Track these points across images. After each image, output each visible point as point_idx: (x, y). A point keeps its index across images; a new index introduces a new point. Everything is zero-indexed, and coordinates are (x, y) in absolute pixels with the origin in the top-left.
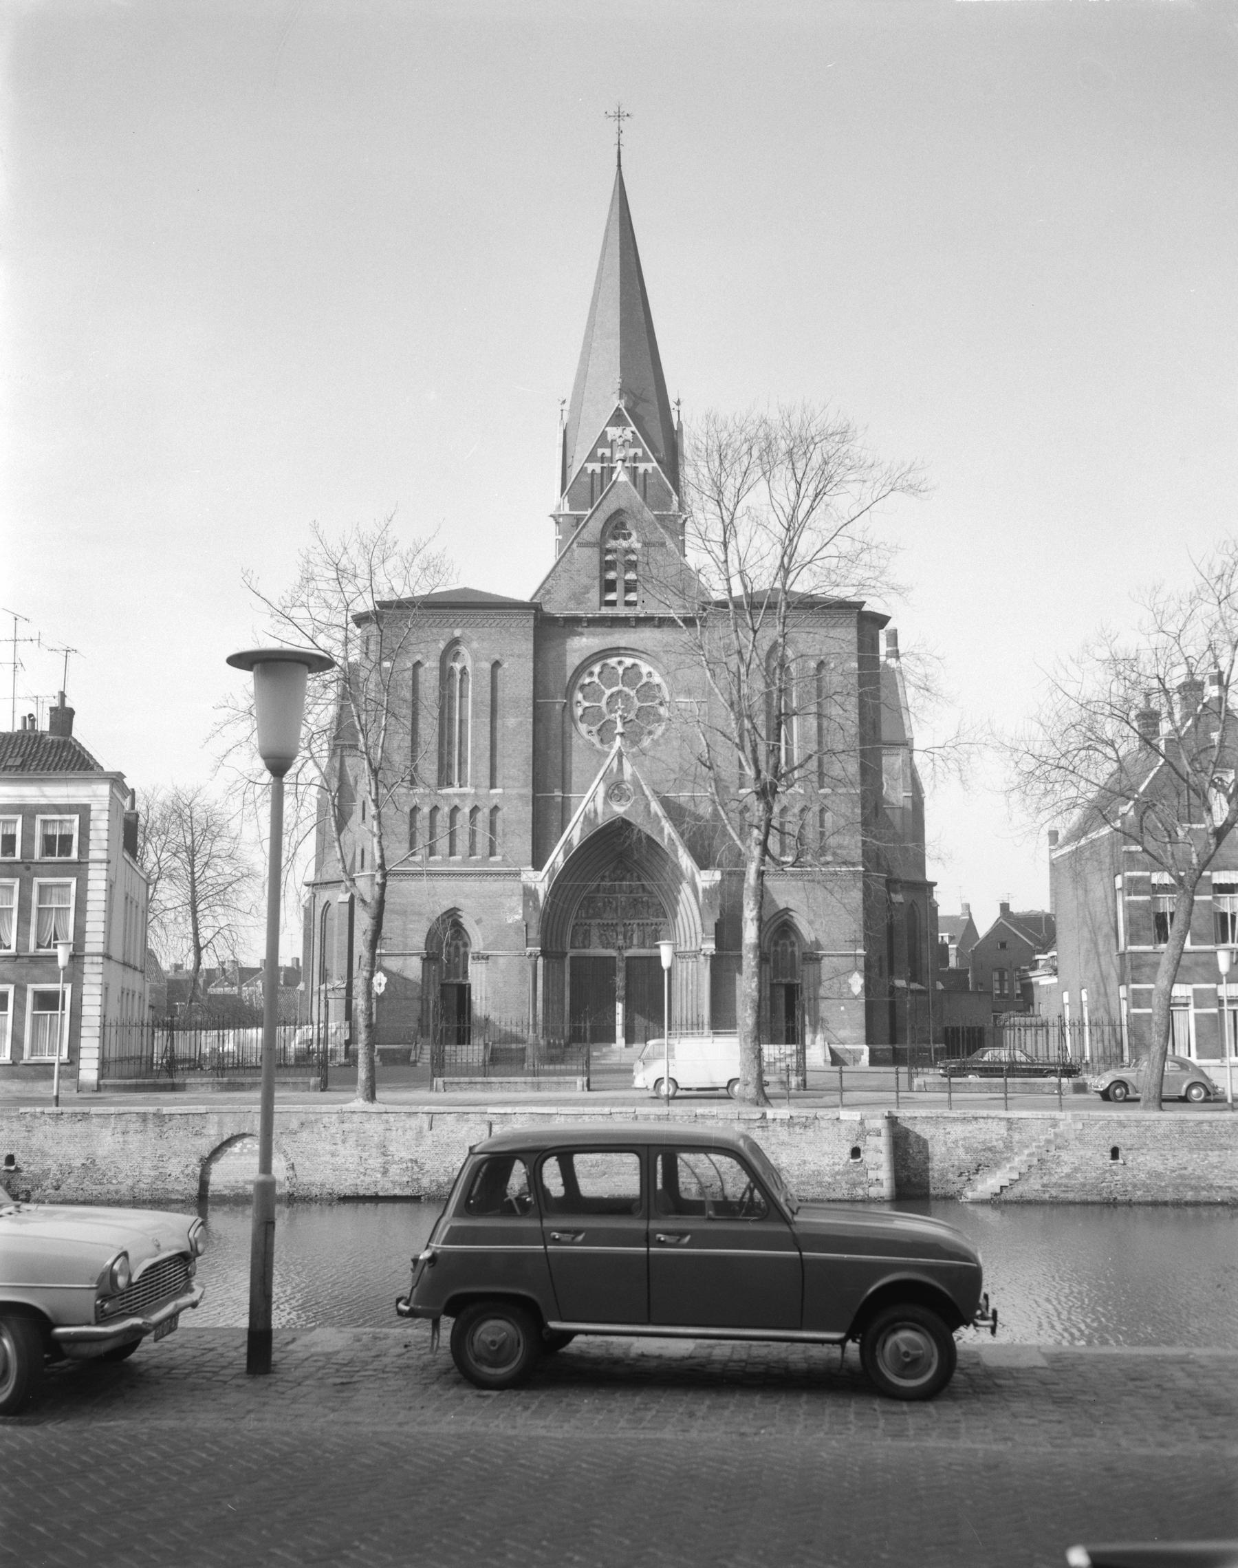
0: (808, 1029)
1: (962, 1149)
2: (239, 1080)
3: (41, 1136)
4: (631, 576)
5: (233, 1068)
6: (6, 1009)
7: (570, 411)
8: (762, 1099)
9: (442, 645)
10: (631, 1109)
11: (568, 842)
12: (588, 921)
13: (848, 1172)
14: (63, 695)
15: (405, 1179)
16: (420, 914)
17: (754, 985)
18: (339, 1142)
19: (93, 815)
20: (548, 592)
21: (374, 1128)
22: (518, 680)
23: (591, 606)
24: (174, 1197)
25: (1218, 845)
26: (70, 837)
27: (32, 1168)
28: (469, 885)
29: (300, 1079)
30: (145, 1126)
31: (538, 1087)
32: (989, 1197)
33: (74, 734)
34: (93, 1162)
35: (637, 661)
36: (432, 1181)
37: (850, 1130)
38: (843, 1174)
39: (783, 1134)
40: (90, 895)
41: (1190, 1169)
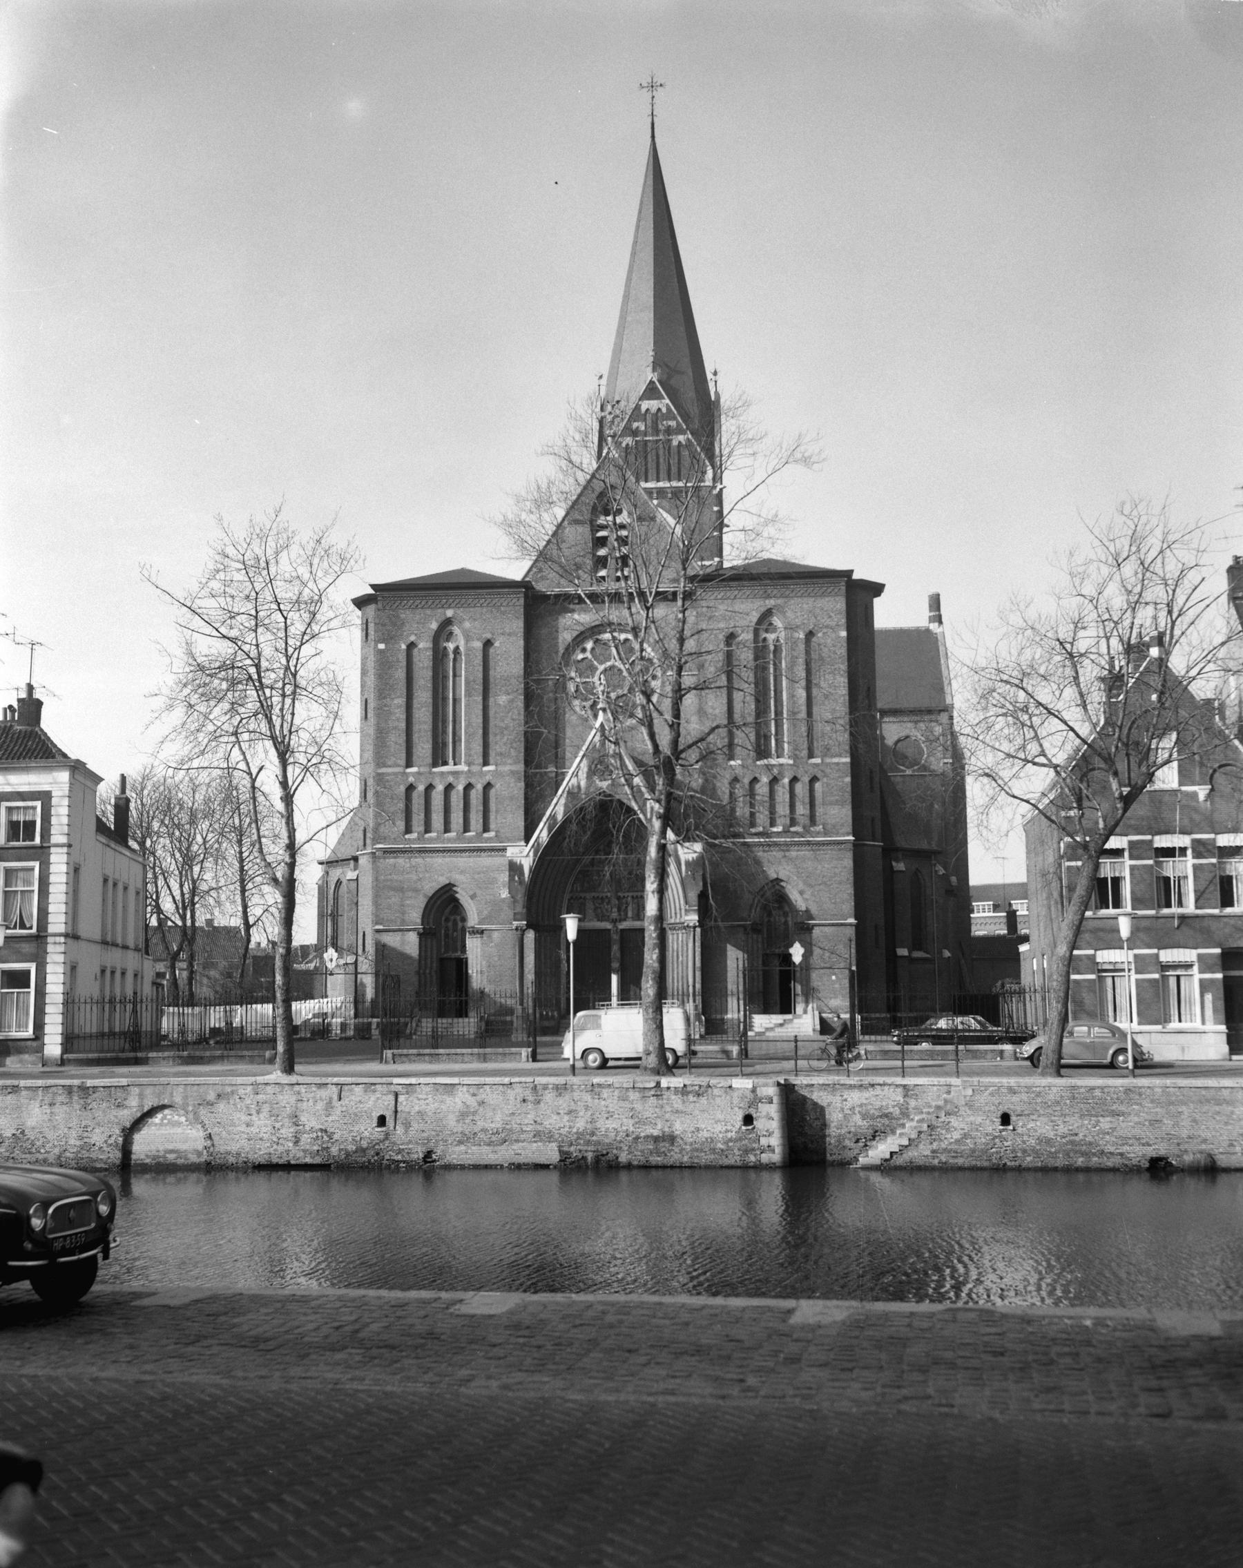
0: (799, 999)
1: (858, 1116)
2: (198, 1053)
5: (175, 1045)
6: (29, 987)
8: (664, 1068)
9: (434, 626)
10: (530, 1079)
11: (553, 817)
12: (582, 895)
13: (740, 1139)
14: (30, 688)
15: (316, 1148)
16: (416, 890)
17: (655, 957)
18: (254, 1112)
19: (54, 801)
21: (287, 1099)
22: (835, 637)
24: (98, 1166)
25: (1125, 810)
26: (34, 823)
28: (463, 861)
29: (256, 1053)
31: (484, 1058)
32: (879, 1162)
33: (43, 725)
34: (23, 1133)
37: (743, 1097)
38: (736, 1140)
39: (677, 1101)
40: (52, 879)
41: (1081, 1135)
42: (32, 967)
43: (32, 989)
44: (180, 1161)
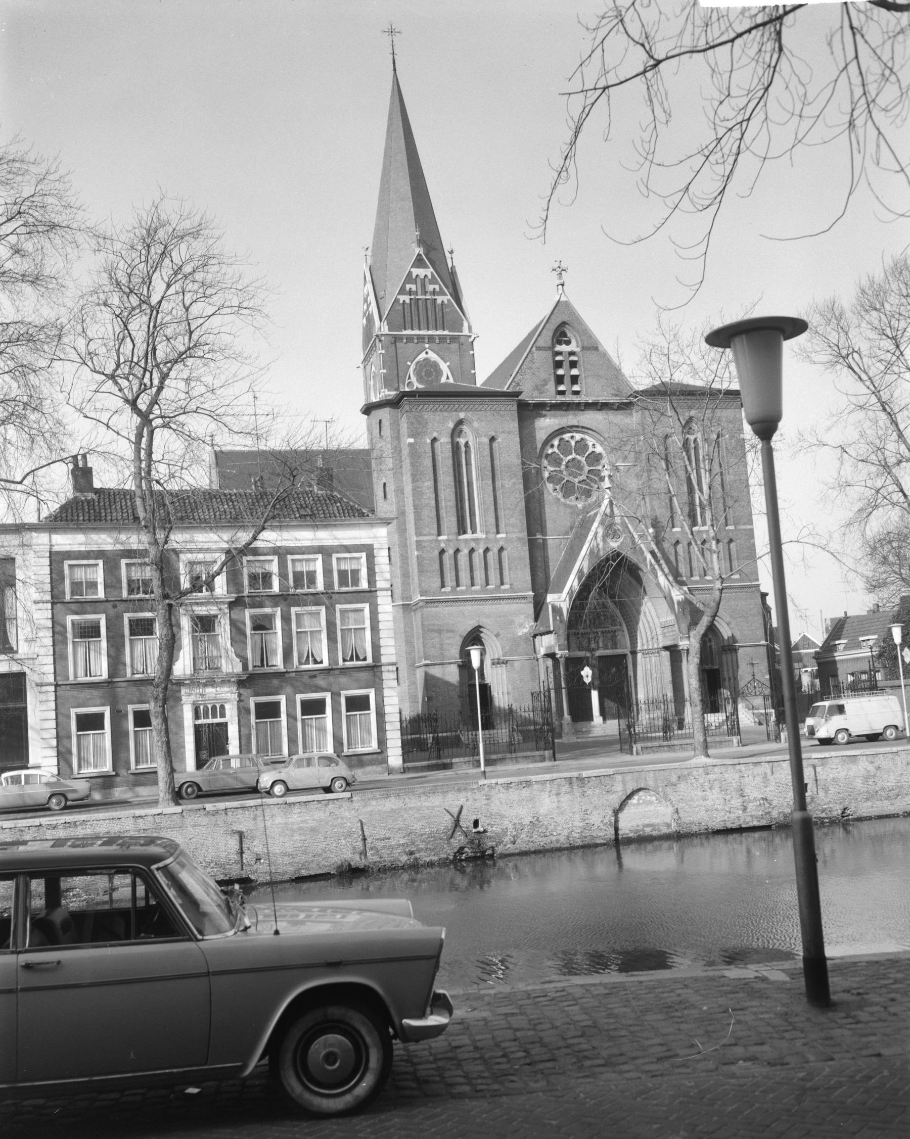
3: (498, 803)
4: (574, 372)
6: (103, 728)
7: (373, 255)
9: (451, 425)
15: (760, 813)
20: (518, 384)
21: (731, 776)
23: (549, 396)
24: (598, 841)
27: (494, 828)
28: (488, 608)
30: (572, 788)
34: (537, 820)
35: (587, 437)
36: (779, 813)
42: (372, 693)
43: (284, 717)
44: (655, 833)
